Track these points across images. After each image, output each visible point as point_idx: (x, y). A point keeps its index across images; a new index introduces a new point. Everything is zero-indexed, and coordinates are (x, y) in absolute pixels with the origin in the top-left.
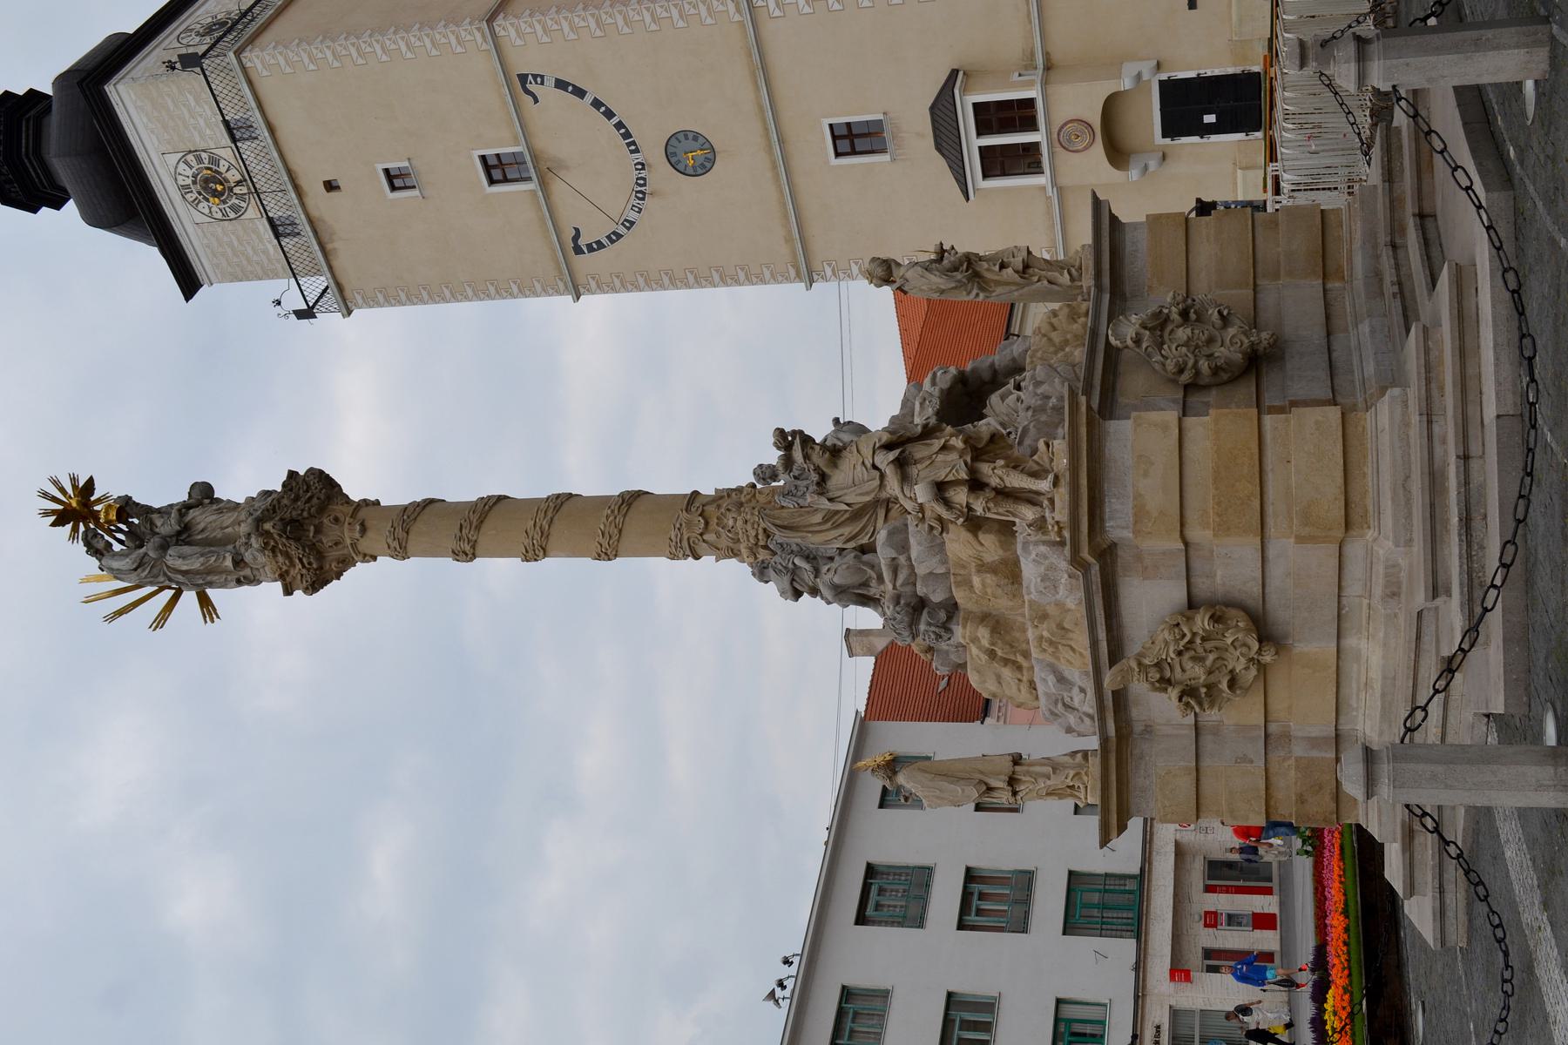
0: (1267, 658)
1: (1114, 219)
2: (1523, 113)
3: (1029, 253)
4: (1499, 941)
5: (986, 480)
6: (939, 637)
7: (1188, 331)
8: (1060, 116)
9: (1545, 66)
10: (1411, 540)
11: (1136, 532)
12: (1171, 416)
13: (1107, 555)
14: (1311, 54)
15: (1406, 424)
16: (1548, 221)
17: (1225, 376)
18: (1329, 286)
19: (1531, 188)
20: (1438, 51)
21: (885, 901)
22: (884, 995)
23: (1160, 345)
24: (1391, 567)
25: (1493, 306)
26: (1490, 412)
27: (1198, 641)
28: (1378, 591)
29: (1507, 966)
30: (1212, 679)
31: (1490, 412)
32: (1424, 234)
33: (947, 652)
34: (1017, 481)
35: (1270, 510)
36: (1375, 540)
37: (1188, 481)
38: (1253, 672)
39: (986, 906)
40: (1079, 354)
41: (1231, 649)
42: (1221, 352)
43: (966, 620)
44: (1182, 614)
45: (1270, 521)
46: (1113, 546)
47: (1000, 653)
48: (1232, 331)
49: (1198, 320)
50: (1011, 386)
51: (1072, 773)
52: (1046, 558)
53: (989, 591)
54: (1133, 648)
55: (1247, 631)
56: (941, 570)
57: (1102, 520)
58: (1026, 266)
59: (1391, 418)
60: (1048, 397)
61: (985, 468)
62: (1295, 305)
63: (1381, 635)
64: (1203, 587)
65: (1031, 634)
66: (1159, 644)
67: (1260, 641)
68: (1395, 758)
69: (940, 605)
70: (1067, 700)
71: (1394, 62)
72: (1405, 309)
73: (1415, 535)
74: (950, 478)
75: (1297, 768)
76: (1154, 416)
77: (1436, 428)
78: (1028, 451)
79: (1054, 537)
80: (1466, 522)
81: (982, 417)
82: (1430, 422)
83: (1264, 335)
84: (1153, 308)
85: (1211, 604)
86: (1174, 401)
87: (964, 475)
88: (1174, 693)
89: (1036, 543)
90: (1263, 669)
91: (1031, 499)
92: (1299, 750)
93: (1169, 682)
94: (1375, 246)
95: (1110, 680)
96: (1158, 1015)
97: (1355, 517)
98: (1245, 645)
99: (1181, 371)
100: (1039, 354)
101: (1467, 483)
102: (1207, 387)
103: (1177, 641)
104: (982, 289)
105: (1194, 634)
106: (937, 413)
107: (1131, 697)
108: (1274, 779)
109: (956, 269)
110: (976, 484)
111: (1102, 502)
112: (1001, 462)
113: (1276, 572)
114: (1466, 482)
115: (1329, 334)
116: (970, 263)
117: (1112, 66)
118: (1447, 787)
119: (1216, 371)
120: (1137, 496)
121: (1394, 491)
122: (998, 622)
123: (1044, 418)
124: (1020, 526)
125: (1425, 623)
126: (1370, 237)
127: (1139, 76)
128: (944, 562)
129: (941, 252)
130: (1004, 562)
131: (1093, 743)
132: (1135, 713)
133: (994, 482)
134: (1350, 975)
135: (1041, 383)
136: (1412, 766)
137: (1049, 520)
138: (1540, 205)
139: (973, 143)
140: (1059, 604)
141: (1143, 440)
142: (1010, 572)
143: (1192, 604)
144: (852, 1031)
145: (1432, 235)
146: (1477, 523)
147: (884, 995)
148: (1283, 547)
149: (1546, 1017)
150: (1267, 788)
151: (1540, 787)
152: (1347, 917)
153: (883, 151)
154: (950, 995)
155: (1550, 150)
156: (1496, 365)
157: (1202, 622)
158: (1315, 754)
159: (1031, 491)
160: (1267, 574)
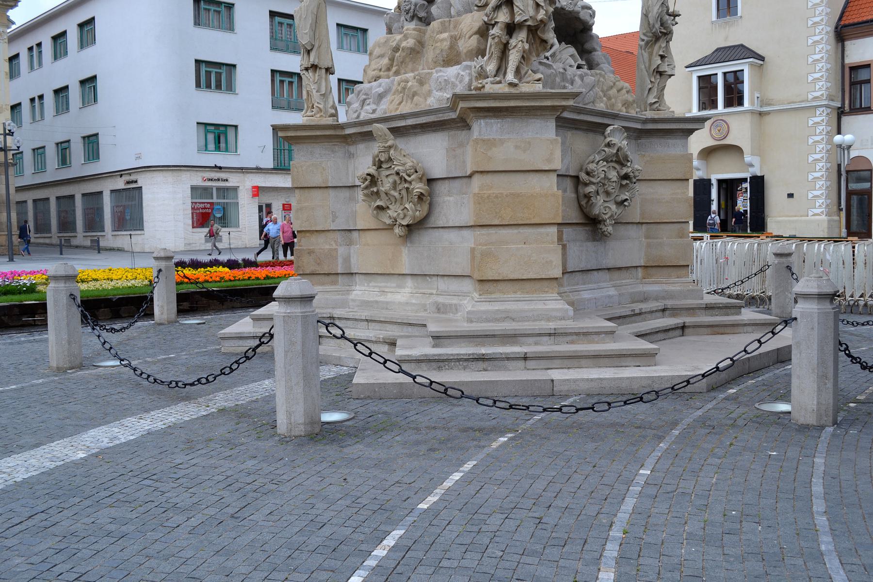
0: (397, 230)
1: (691, 131)
2: (762, 401)
3: (670, 76)
4: (199, 380)
5: (514, 35)
6: (407, 12)
7: (615, 179)
8: (731, 121)
9: (802, 421)
10: (472, 322)
11: (476, 141)
12: (557, 165)
13: (462, 123)
14: (783, 260)
15: (549, 319)
16: (688, 420)
17: (583, 203)
18: (640, 270)
19: (710, 406)
20: (821, 350)
21: (285, 27)
22: (231, 28)
23: (605, 160)
24: (455, 308)
25: (628, 378)
26: (556, 375)
27: (406, 185)
28: (441, 299)
29: (186, 385)
30: (383, 195)
31: (556, 375)
32: (672, 329)
33: (399, 21)
34: (514, 58)
35: (492, 231)
36: (473, 298)
37: (513, 175)
38: (388, 221)
39: (286, 85)
40: (601, 106)
41: (402, 207)
42: (599, 201)
43: (419, 31)
44: (423, 175)
45: (484, 231)
46: (468, 127)
47: (397, 54)
48: (614, 207)
49: (622, 186)
50: (580, 62)
51: (321, 106)
52: (461, 82)
53: (438, 44)
54: (403, 144)
55: (414, 217)
56: (453, 12)
57: (485, 117)
58: (661, 74)
59: (553, 310)
60: (572, 84)
61: (523, 35)
62: (627, 248)
63: (414, 301)
64: (441, 188)
65: (410, 75)
66: (403, 160)
67: (408, 226)
68: (305, 317)
69: (429, 13)
70: (368, 101)
71: (816, 319)
72: (625, 317)
73: (474, 324)
74: (516, 9)
75: (331, 250)
76: (558, 153)
77: (546, 339)
78: (535, 69)
79: (475, 84)
80: (482, 358)
81: (560, 42)
82: (550, 335)
83: (610, 229)
84: (631, 157)
85: (431, 194)
86: (567, 169)
87: (518, 19)
88: (372, 170)
89: (470, 74)
90: (391, 228)
91: (501, 69)
92: (342, 250)
93: (380, 167)
94: (664, 298)
95: (382, 127)
96: (234, 180)
97: (487, 286)
98: (405, 216)
99: (588, 174)
100: (602, 79)
101: (508, 359)
102: (577, 191)
103: (405, 171)
104: (647, 43)
105: (410, 183)
106: (562, 9)
107: (371, 144)
108: (323, 235)
109: (662, 25)
110: (511, 28)
111: (497, 117)
112: (527, 46)
113: (452, 235)
114: (509, 358)
115: (609, 269)
116: (665, 34)
117: (758, 151)
118: (286, 352)
119: (588, 197)
120: (502, 142)
121: (505, 311)
122: (418, 52)
123: (558, 80)
124: (481, 61)
125: (419, 328)
126: (671, 295)
127: (751, 165)
128: (459, 14)
129: (675, 15)
130: (458, 54)
131: (342, 119)
132: (361, 147)
133: (513, 42)
134: (231, 280)
135: (582, 80)
136: (299, 328)
137: (485, 81)
138: (699, 413)
139: (719, 71)
140: (429, 93)
141: (542, 145)
142: (451, 59)
143: (430, 181)
144: (209, 10)
145: (671, 334)
146: (481, 365)
147: (231, 28)
148: (468, 240)
149: (147, 411)
150: (317, 231)
151: (289, 414)
152: (265, 279)
153: (718, 16)
154: (234, 66)
155: (740, 422)
156: (587, 380)
157: (419, 187)
158: (340, 260)
159: (506, 69)
160: (451, 230)
